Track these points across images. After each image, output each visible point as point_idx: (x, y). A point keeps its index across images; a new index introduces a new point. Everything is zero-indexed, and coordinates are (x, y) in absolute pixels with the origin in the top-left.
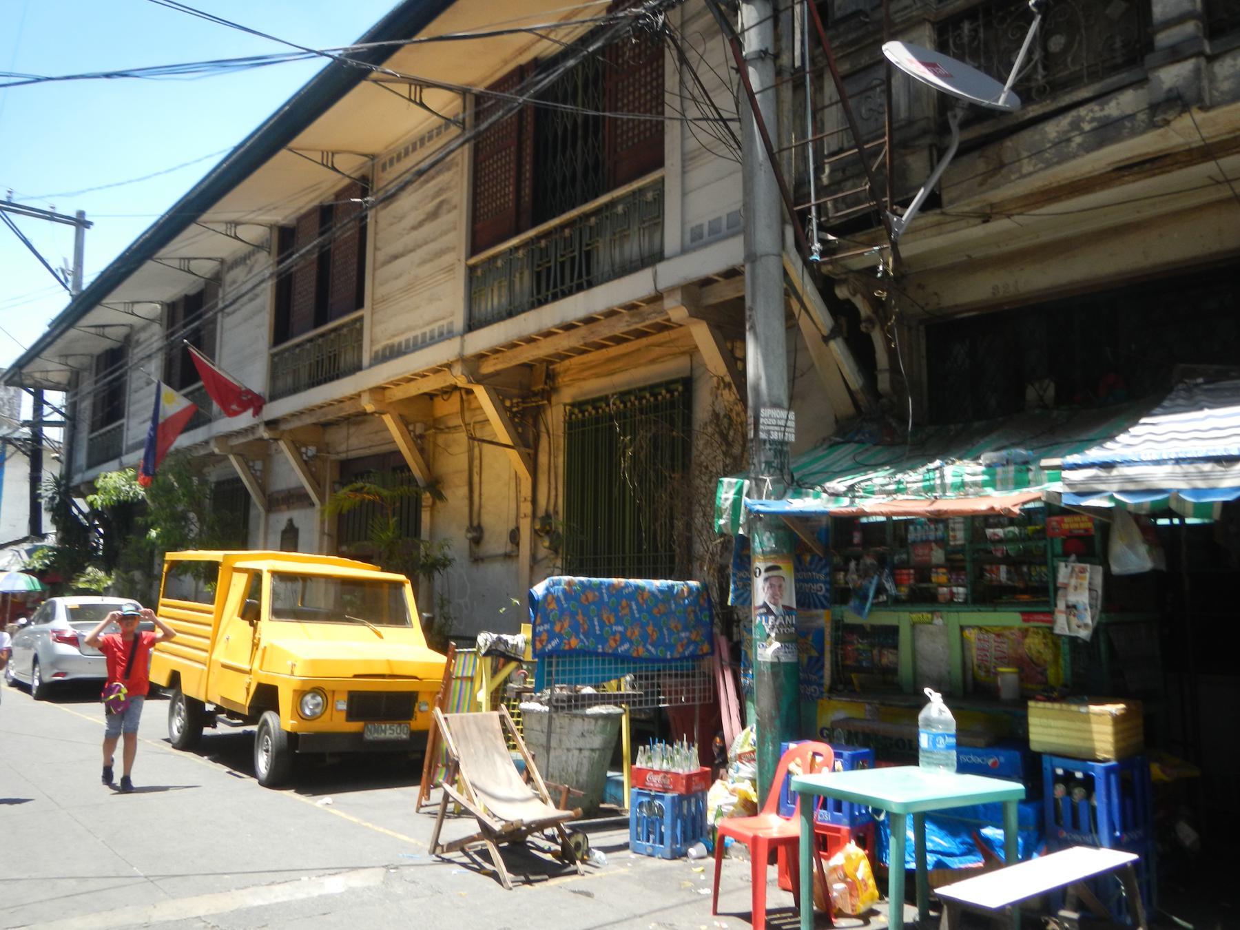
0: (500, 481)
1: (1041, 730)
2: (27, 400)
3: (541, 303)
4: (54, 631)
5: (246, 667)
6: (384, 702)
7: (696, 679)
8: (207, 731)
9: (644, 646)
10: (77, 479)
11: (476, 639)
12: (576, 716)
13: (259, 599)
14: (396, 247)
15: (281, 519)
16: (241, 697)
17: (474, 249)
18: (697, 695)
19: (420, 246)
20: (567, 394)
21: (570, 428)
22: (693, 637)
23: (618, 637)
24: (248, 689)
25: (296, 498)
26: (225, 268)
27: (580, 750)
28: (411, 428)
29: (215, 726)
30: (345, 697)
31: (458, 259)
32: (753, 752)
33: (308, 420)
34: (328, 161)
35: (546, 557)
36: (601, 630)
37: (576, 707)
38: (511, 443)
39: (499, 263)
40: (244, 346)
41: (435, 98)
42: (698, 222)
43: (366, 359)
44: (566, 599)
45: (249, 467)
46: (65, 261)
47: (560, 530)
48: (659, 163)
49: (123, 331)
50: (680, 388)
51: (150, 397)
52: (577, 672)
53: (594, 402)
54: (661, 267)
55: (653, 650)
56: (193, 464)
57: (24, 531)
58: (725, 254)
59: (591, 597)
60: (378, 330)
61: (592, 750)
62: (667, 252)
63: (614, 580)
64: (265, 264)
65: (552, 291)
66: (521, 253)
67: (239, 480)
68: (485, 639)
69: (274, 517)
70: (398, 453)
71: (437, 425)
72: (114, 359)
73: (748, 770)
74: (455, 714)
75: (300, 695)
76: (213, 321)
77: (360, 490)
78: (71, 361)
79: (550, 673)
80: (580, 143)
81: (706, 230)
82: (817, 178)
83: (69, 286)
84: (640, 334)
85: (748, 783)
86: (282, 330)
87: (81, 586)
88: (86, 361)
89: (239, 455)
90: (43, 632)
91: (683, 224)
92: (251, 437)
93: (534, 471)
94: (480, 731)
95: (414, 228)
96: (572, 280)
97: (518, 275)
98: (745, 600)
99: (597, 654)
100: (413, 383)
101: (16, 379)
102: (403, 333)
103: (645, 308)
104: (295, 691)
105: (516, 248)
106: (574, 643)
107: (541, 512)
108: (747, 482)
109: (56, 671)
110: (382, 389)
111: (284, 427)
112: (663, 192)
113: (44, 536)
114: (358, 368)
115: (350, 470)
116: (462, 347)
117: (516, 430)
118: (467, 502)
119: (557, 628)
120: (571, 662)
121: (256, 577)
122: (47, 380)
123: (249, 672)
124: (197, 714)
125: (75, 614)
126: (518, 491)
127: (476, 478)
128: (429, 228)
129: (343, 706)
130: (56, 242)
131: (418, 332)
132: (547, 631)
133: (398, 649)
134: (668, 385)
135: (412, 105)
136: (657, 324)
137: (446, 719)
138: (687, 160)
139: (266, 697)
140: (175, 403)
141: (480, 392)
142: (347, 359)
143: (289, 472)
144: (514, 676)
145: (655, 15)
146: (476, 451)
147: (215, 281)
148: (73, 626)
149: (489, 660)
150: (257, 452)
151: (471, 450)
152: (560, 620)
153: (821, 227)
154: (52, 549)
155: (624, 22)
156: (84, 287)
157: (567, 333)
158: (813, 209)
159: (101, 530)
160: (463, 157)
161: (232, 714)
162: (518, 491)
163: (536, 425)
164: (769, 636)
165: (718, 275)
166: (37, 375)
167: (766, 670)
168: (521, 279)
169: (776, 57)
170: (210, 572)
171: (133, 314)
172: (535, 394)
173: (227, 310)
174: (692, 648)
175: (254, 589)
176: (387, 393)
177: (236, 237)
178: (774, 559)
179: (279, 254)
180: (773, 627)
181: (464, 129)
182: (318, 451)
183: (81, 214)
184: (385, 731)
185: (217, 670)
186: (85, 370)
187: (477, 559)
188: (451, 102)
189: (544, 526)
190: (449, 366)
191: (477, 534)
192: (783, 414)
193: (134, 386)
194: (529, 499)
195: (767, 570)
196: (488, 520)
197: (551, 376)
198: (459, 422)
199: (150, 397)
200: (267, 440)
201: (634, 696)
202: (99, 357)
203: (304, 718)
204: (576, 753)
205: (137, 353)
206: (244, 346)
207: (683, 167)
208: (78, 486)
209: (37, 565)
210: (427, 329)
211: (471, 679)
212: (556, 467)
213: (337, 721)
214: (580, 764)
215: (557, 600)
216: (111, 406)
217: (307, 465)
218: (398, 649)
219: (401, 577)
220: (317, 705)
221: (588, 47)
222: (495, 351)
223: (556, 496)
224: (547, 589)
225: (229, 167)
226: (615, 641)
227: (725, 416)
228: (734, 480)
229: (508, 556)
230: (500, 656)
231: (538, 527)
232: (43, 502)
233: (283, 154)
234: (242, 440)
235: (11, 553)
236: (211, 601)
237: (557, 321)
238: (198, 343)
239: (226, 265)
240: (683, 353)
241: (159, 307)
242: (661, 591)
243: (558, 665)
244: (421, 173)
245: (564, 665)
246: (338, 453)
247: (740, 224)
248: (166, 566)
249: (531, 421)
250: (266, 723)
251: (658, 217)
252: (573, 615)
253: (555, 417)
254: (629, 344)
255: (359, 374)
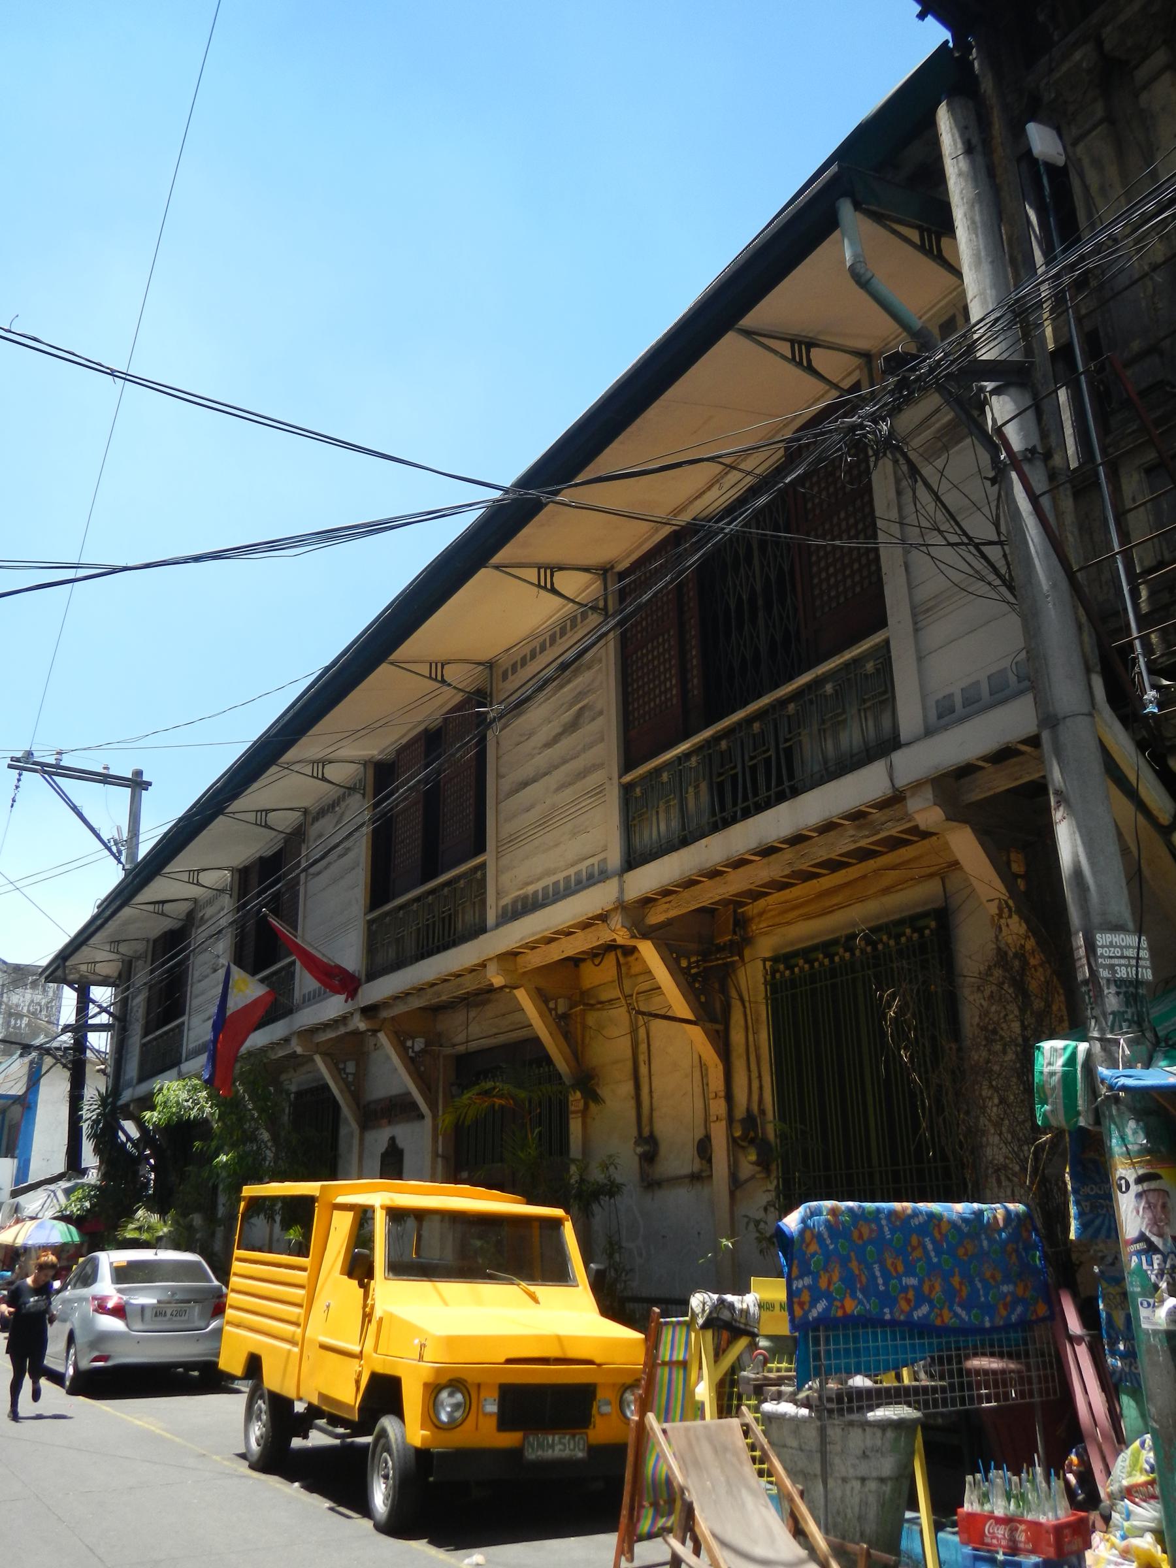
0: (678, 1071)
1: (675, 1354)
2: (69, 997)
3: (727, 823)
4: (94, 1298)
5: (356, 1349)
6: (544, 1399)
7: (1032, 1361)
8: (297, 1443)
9: (951, 1310)
10: (127, 1096)
11: (686, 1302)
12: (851, 1424)
13: (372, 1249)
14: (528, 770)
15: (379, 1139)
16: (347, 1393)
17: (628, 765)
18: (1035, 1387)
19: (556, 767)
20: (765, 946)
21: (774, 990)
22: (1020, 1291)
23: (911, 1295)
24: (358, 1382)
25: (399, 1109)
26: (310, 819)
27: (863, 1480)
28: (552, 1005)
29: (306, 1437)
30: (496, 1394)
31: (607, 778)
32: (1152, 1483)
33: (416, 1003)
34: (437, 672)
35: (752, 1177)
36: (885, 1284)
37: (850, 1410)
38: (691, 1017)
39: (665, 777)
40: (334, 914)
41: (570, 583)
42: (946, 692)
43: (491, 918)
44: (831, 1236)
45: (339, 1070)
46: (119, 829)
47: (771, 1135)
48: (881, 622)
49: (185, 907)
50: (933, 924)
51: (219, 983)
52: (857, 1352)
53: (806, 953)
54: (898, 757)
55: (963, 1314)
56: (268, 1070)
57: (60, 1166)
58: (1012, 721)
59: (865, 1231)
60: (505, 878)
61: (882, 1480)
62: (904, 736)
63: (897, 1206)
64: (359, 810)
65: (740, 805)
66: (694, 761)
67: (326, 1087)
68: (699, 1301)
69: (370, 1136)
70: (537, 1040)
71: (586, 1000)
72: (174, 943)
73: (1147, 1513)
74: (678, 1424)
75: (433, 1391)
76: (296, 882)
77: (487, 1093)
78: (123, 948)
79: (817, 1356)
80: (761, 614)
81: (958, 700)
82: (1136, 606)
83: (123, 859)
84: (865, 855)
85: (1149, 1538)
86: (380, 889)
87: (129, 1235)
88: (140, 947)
89: (325, 1055)
90: (82, 1299)
91: (924, 697)
92: (342, 1030)
93: (725, 1052)
94: (716, 1451)
95: (548, 745)
96: (768, 789)
97: (691, 790)
98: (1109, 1229)
99: (883, 1324)
100: (553, 945)
101: (59, 973)
102: (539, 879)
103: (876, 815)
104: (426, 1385)
105: (687, 755)
106: (851, 1306)
107: (740, 1112)
108: (1083, 1047)
109: (96, 1354)
110: (513, 954)
111: (385, 1014)
112: (889, 659)
113: (83, 1172)
114: (482, 929)
115: (471, 1068)
116: (622, 890)
117: (698, 999)
118: (633, 1103)
119: (823, 1284)
120: (846, 1337)
121: (364, 1216)
122: (94, 973)
123: (359, 1356)
124: (284, 1419)
125: (122, 1274)
126: (705, 1084)
127: (643, 1070)
128: (566, 743)
129: (492, 1408)
130: (109, 808)
131: (560, 876)
132: (809, 1288)
133: (561, 1318)
134: (913, 920)
135: (543, 593)
136: (890, 837)
137: (664, 1431)
138: (919, 615)
139: (384, 1393)
140: (248, 990)
141: (648, 952)
142: (468, 917)
143: (391, 1074)
144: (746, 1358)
145: (875, 422)
146: (642, 1032)
147: (296, 837)
148: (119, 1291)
149: (709, 1334)
150: (349, 1049)
151: (634, 1031)
152: (826, 1270)
153: (1151, 672)
154: (94, 1187)
155: (836, 437)
156: (140, 859)
157: (765, 860)
158: (1137, 643)
159: (152, 1161)
160: (607, 654)
161: (335, 1420)
162: (705, 1084)
163: (724, 990)
164: (1156, 1287)
165: (985, 758)
166: (84, 968)
167: (1158, 1343)
168: (697, 794)
169: (1048, 456)
170: (300, 1213)
171: (198, 884)
172: (720, 949)
173: (312, 870)
174: (1019, 1309)
175: (362, 1236)
176: (520, 959)
177: (324, 779)
178: (1148, 1163)
179: (376, 792)
180: (1161, 1274)
181: (607, 616)
182: (427, 1044)
183: (139, 773)
184: (552, 1446)
185: (312, 1352)
186: (138, 958)
187: (651, 1184)
188: (591, 585)
189: (746, 1133)
190: (603, 917)
191: (649, 1147)
192: (1132, 940)
193: (197, 974)
194: (722, 1094)
195: (1140, 1180)
196: (664, 1128)
197: (741, 923)
198: (616, 993)
199: (219, 983)
200: (362, 1033)
201: (934, 1389)
202: (155, 941)
203: (438, 1426)
204: (857, 1485)
205: (200, 935)
206: (334, 914)
207: (915, 623)
208: (127, 1105)
209: (74, 1209)
210: (571, 871)
211: (684, 1365)
212: (757, 1049)
213: (484, 1431)
214: (864, 1503)
215: (819, 1237)
216: (169, 1000)
217: (413, 1063)
218: (561, 1318)
219: (558, 1212)
220: (456, 1407)
221: (785, 477)
222: (666, 893)
223: (761, 1088)
224: (803, 1221)
225: (318, 692)
226: (908, 1301)
227: (1016, 955)
228: (1059, 1044)
229: (698, 1178)
230: (727, 1328)
231: (738, 1134)
232: (85, 1126)
233: (384, 668)
234: (331, 1035)
235: (45, 1195)
236: (302, 1249)
237: (753, 844)
238: (276, 912)
239: (310, 816)
240: (931, 875)
241: (228, 874)
242: (965, 1220)
243: (827, 1342)
244: (564, 667)
245: (836, 1343)
246: (454, 1045)
247: (1029, 678)
248: (242, 1204)
249: (716, 986)
250: (383, 1433)
251: (885, 692)
252: (844, 1262)
253: (751, 978)
254: (850, 870)
255: (482, 937)
